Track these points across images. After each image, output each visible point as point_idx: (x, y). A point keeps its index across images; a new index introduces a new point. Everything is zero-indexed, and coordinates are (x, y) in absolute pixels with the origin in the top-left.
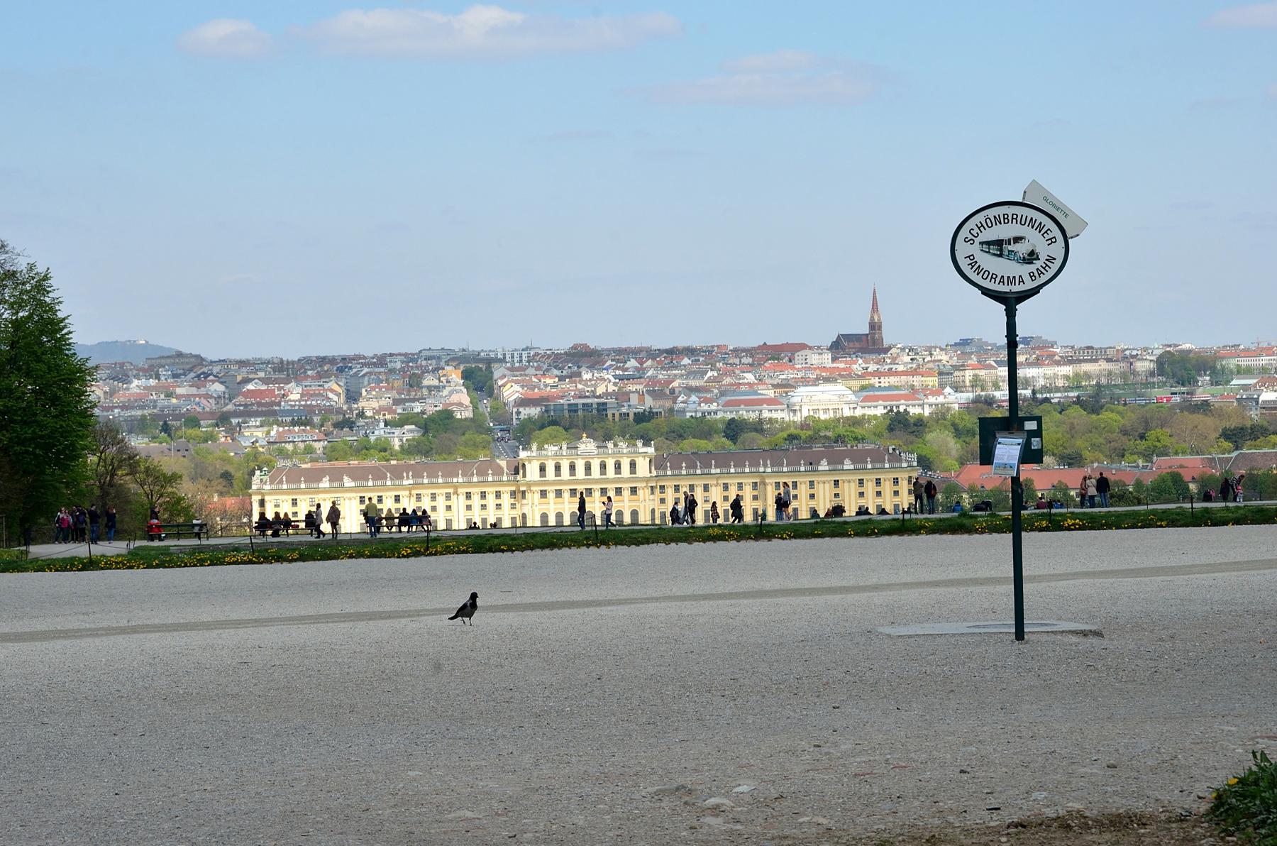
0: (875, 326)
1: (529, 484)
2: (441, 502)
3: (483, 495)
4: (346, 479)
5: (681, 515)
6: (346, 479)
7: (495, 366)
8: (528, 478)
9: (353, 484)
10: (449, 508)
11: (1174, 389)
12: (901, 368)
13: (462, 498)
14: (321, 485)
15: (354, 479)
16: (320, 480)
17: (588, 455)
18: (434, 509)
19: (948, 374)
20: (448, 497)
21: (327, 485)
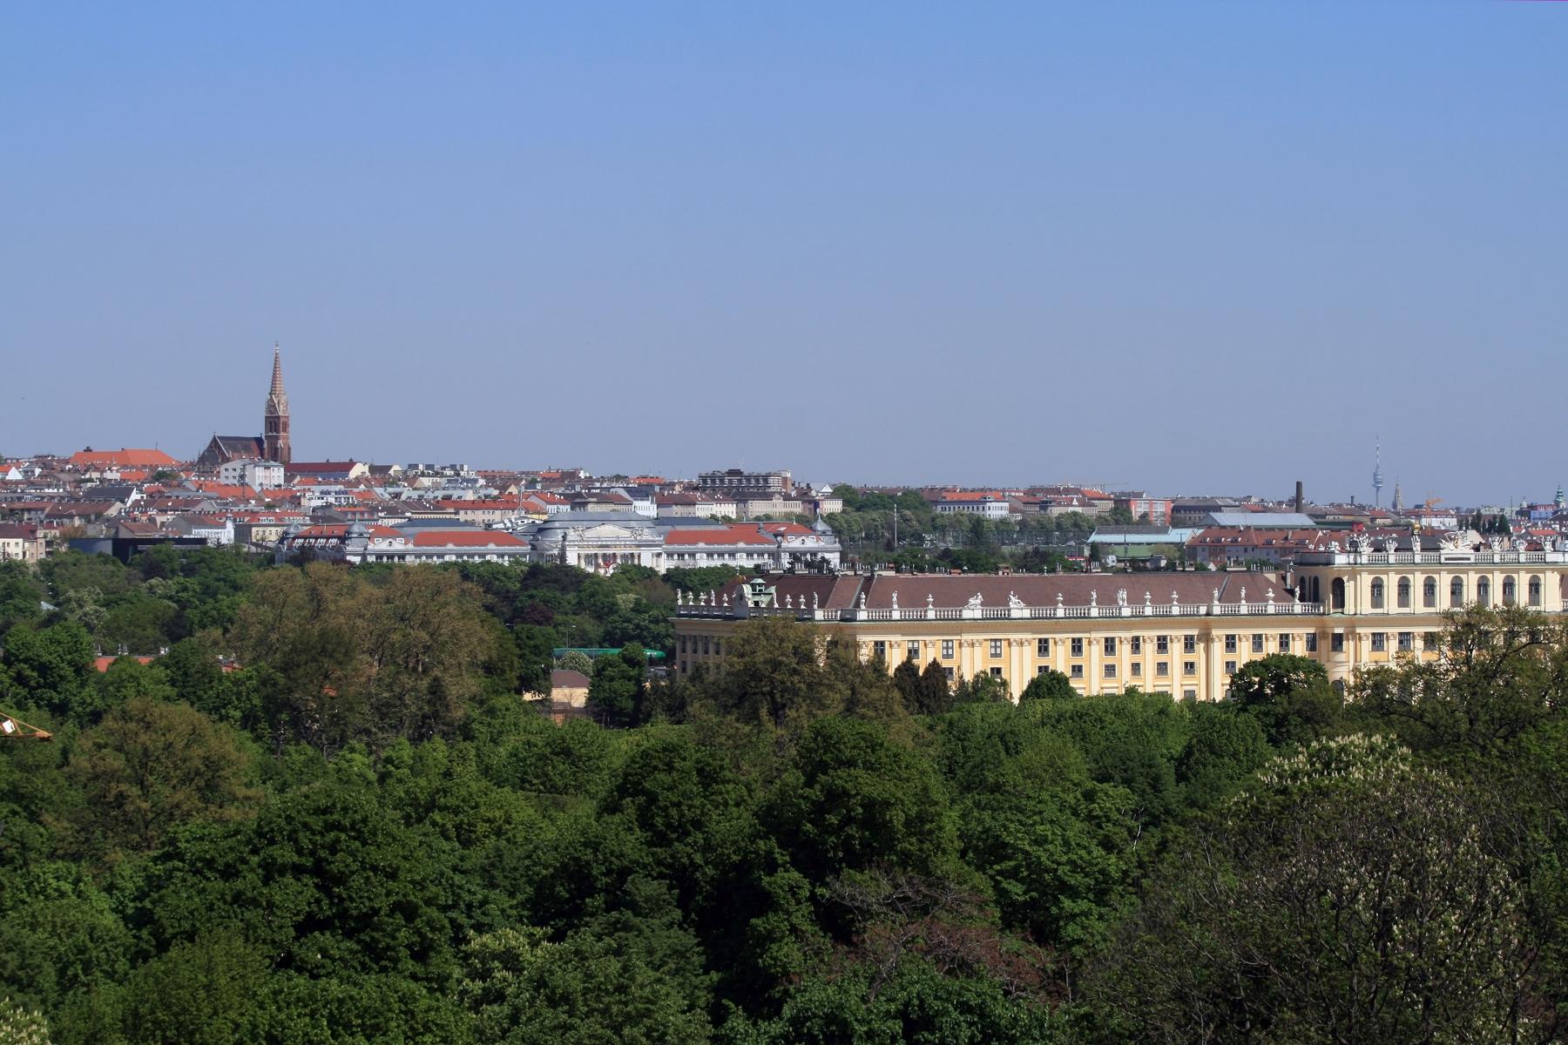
0: (274, 423)
1: (1353, 622)
2: (1094, 656)
3: (1162, 645)
4: (1014, 601)
5: (463, 947)
6: (1014, 601)
7: (771, 480)
8: (1349, 608)
9: (1026, 613)
10: (1190, 667)
11: (325, 488)
12: (470, 496)
13: (1218, 647)
14: (967, 614)
15: (1029, 603)
16: (964, 603)
17: (1457, 563)
18: (1077, 670)
19: (337, 520)
20: (1189, 644)
21: (978, 614)
